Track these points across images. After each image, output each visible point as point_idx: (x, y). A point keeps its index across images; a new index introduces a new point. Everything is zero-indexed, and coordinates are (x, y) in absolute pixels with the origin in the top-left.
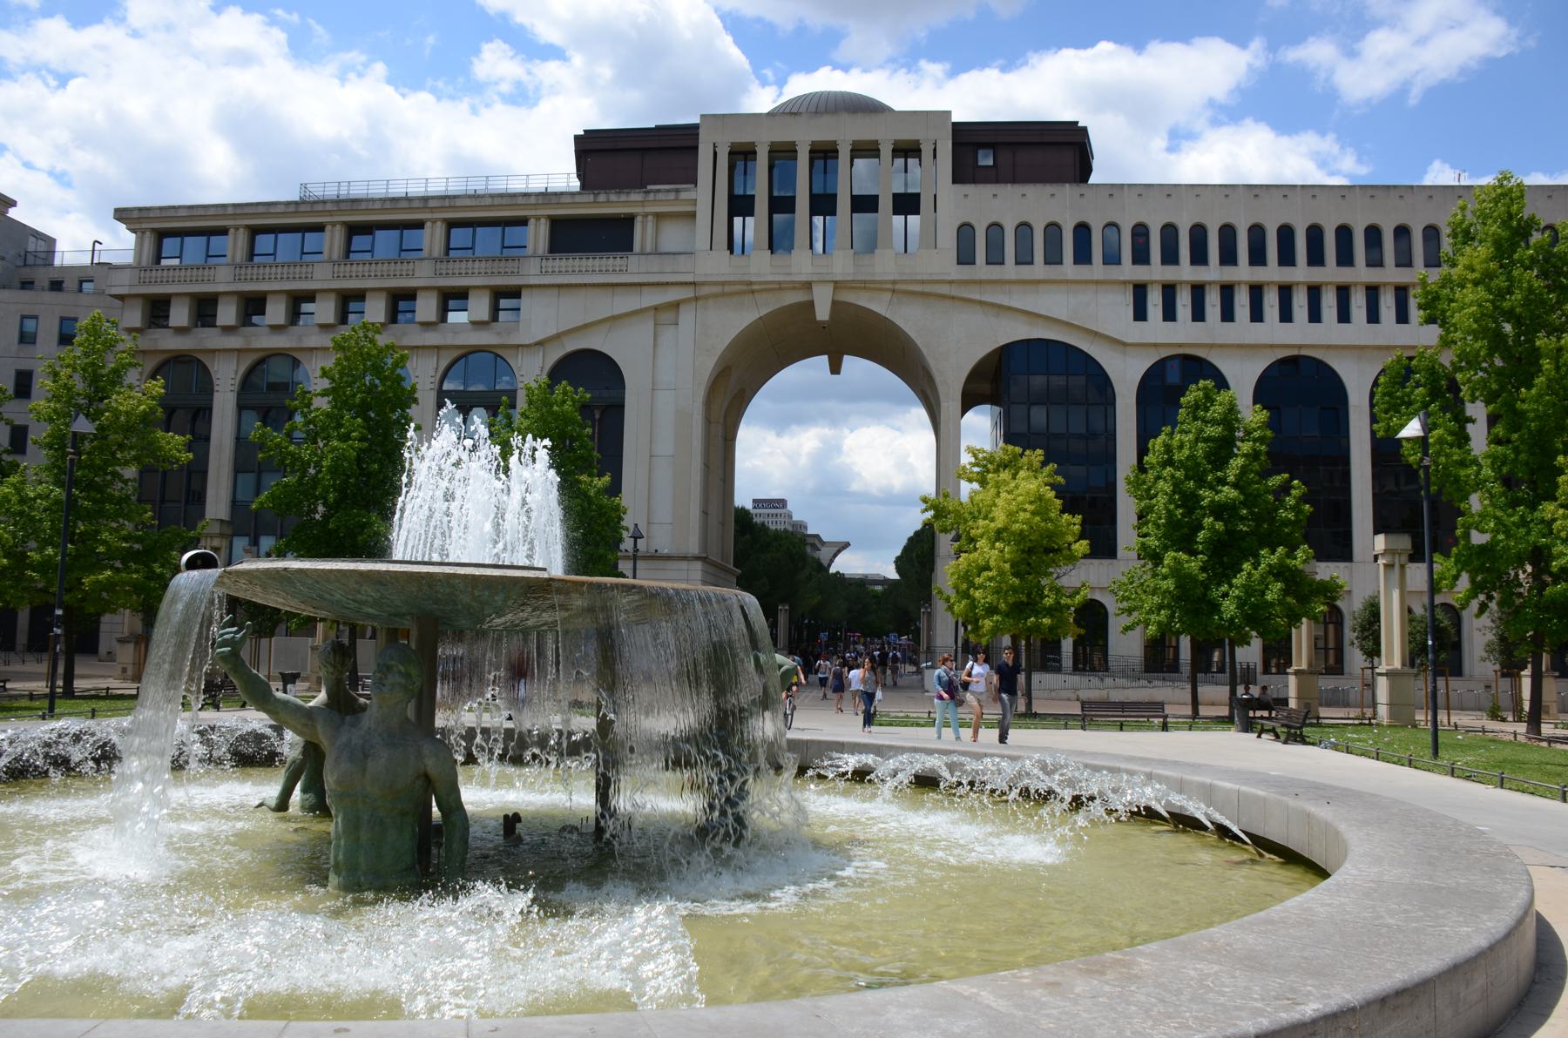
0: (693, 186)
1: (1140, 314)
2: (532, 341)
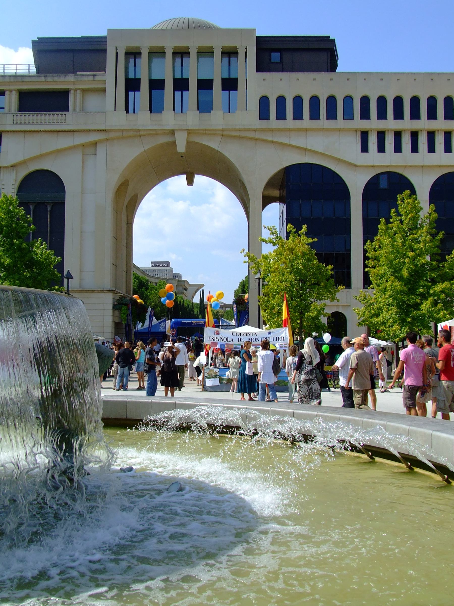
0: (104, 73)
1: (365, 148)
2: (9, 164)
